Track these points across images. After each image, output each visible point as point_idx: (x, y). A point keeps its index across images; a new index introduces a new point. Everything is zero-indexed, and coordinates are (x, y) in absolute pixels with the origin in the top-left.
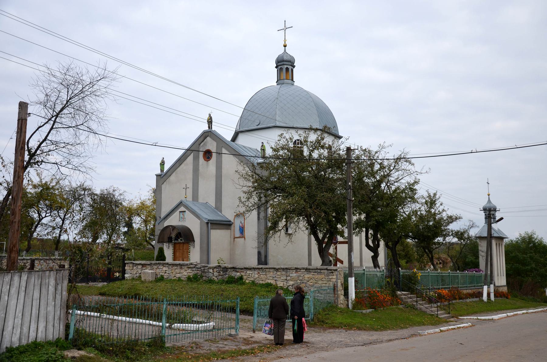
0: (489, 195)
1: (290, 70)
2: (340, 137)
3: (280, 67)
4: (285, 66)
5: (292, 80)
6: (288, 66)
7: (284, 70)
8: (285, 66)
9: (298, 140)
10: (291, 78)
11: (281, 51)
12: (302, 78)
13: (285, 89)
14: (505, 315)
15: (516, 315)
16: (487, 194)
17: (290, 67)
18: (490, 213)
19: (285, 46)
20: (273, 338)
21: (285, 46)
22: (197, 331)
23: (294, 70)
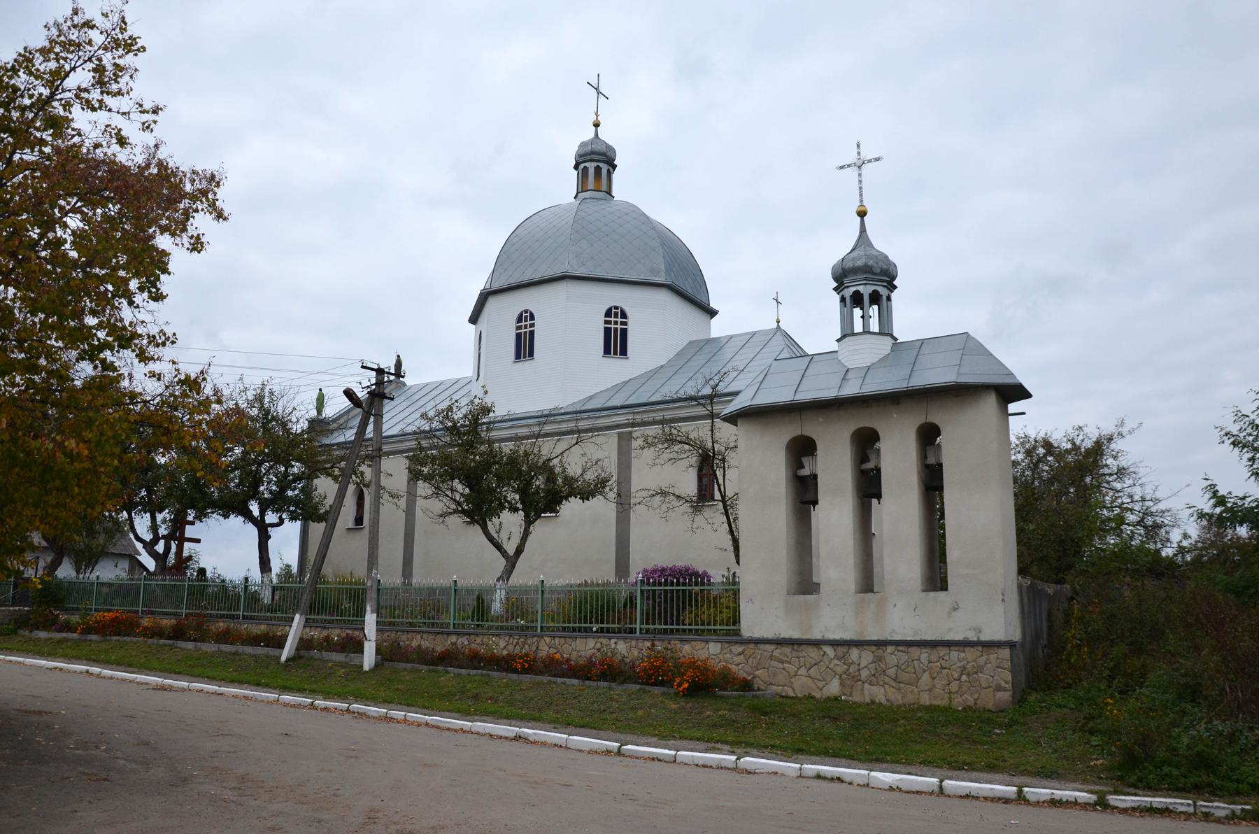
0: (862, 214)
1: (604, 172)
2: (712, 313)
3: (582, 166)
4: (596, 164)
5: (609, 193)
6: (601, 165)
7: (591, 172)
8: (596, 164)
9: (616, 308)
10: (604, 188)
11: (589, 134)
12: (626, 185)
13: (597, 209)
14: (84, 668)
15: (170, 689)
16: (855, 206)
17: (604, 167)
18: (865, 282)
19: (597, 125)
20: (1008, 657)
21: (597, 125)
22: (111, 678)
23: (616, 176)
